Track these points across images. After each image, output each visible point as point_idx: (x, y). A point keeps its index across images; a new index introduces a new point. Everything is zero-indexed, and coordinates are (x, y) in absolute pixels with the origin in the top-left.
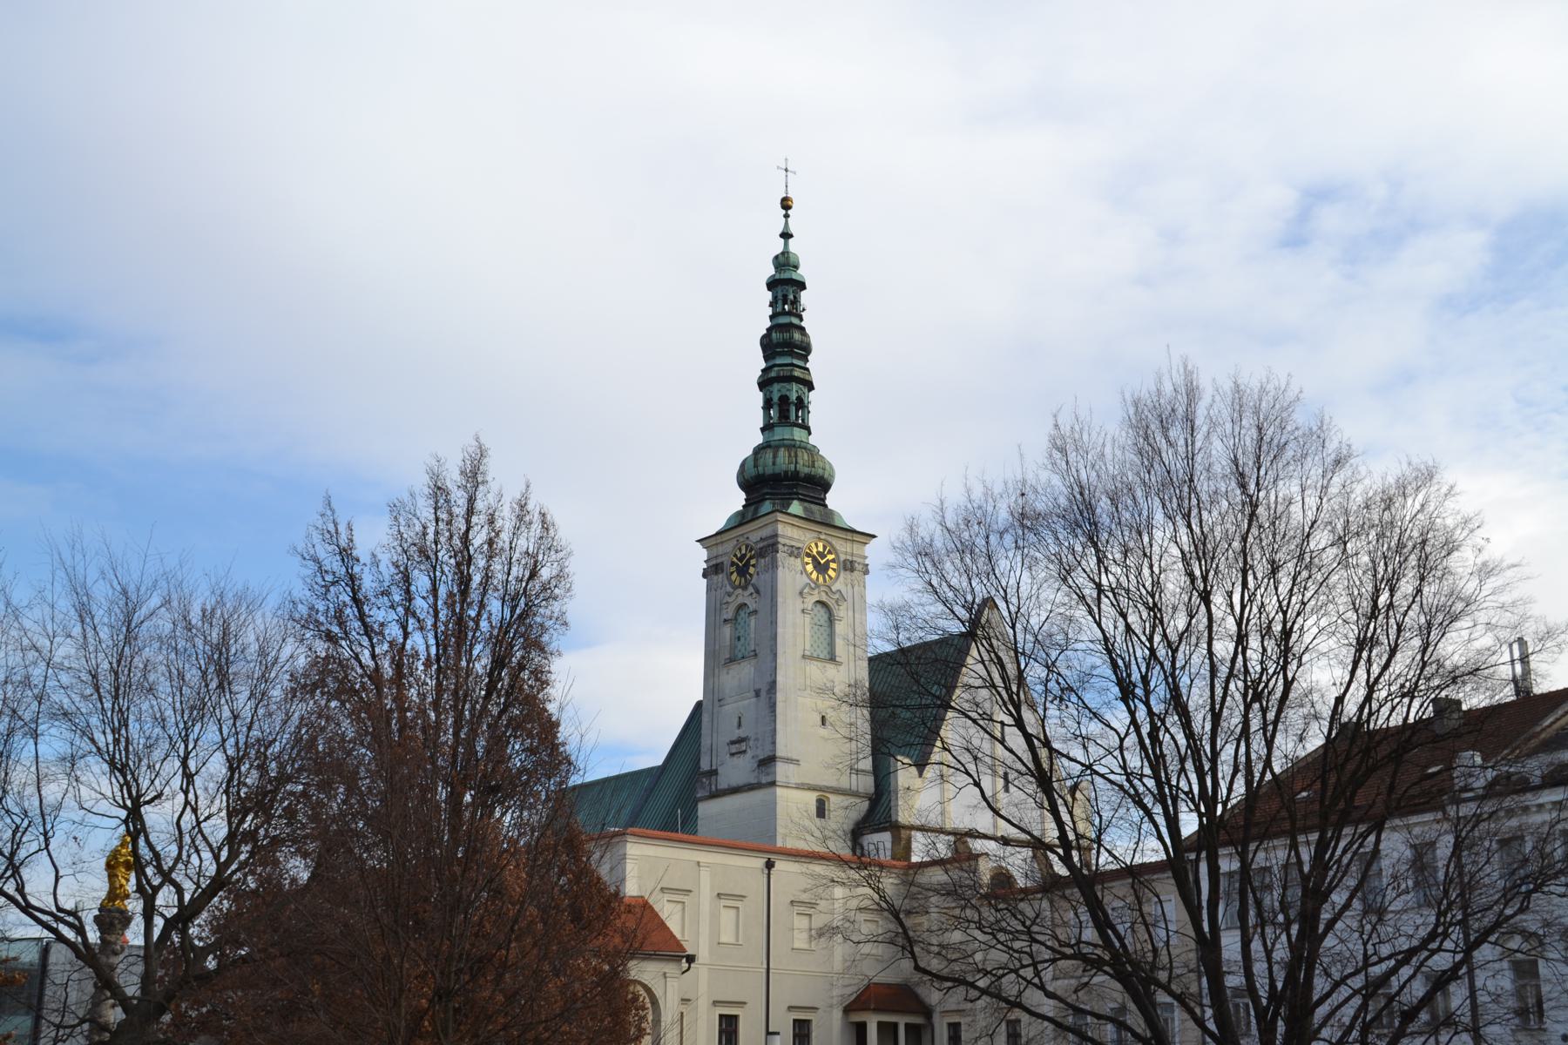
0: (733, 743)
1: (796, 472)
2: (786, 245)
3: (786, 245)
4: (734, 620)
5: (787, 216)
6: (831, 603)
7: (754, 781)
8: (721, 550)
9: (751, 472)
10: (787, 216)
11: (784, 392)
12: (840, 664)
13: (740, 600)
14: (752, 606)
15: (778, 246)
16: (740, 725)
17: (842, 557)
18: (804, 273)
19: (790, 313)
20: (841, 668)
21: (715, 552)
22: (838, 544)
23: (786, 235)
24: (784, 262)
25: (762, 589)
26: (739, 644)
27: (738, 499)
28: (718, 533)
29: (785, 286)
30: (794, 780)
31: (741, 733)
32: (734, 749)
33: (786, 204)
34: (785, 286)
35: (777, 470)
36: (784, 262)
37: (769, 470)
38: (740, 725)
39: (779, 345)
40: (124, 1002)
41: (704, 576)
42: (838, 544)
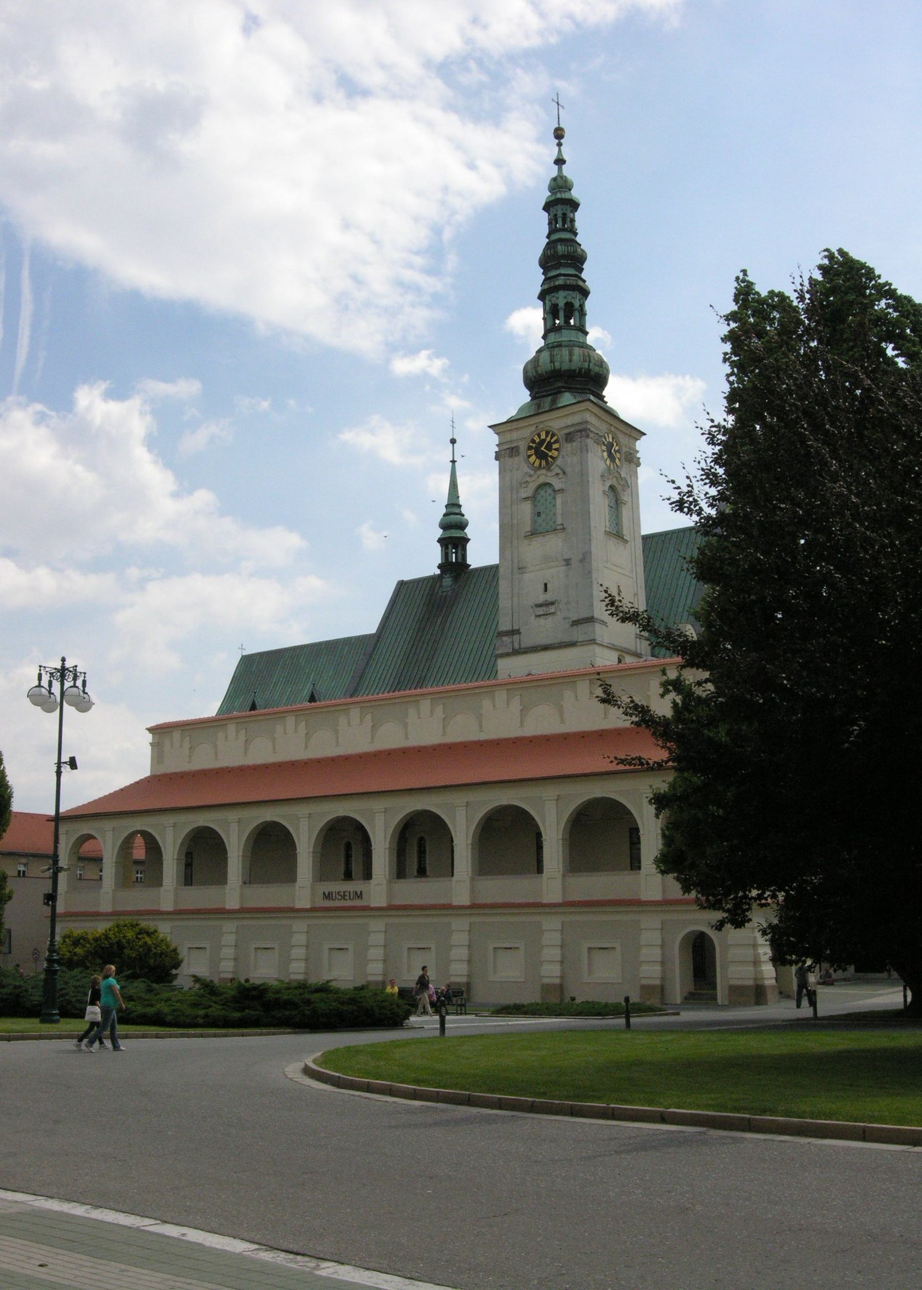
0: (540, 605)
1: (589, 370)
2: (560, 170)
3: (560, 170)
4: (533, 498)
5: (559, 145)
6: (619, 488)
7: (566, 639)
8: (515, 435)
9: (545, 364)
10: (559, 145)
11: (570, 299)
12: (626, 542)
13: (542, 479)
14: (557, 484)
15: (554, 171)
16: (546, 590)
17: (624, 449)
18: (575, 194)
19: (563, 230)
20: (628, 545)
21: (508, 437)
22: (621, 437)
23: (560, 162)
24: (560, 185)
25: (568, 470)
26: (540, 520)
27: (525, 396)
28: (509, 421)
29: (561, 206)
30: (606, 641)
31: (549, 597)
32: (540, 611)
33: (559, 134)
34: (561, 206)
35: (573, 368)
36: (560, 185)
37: (565, 367)
38: (546, 590)
39: (563, 257)
40: (764, 893)
41: (497, 458)
42: (621, 437)
